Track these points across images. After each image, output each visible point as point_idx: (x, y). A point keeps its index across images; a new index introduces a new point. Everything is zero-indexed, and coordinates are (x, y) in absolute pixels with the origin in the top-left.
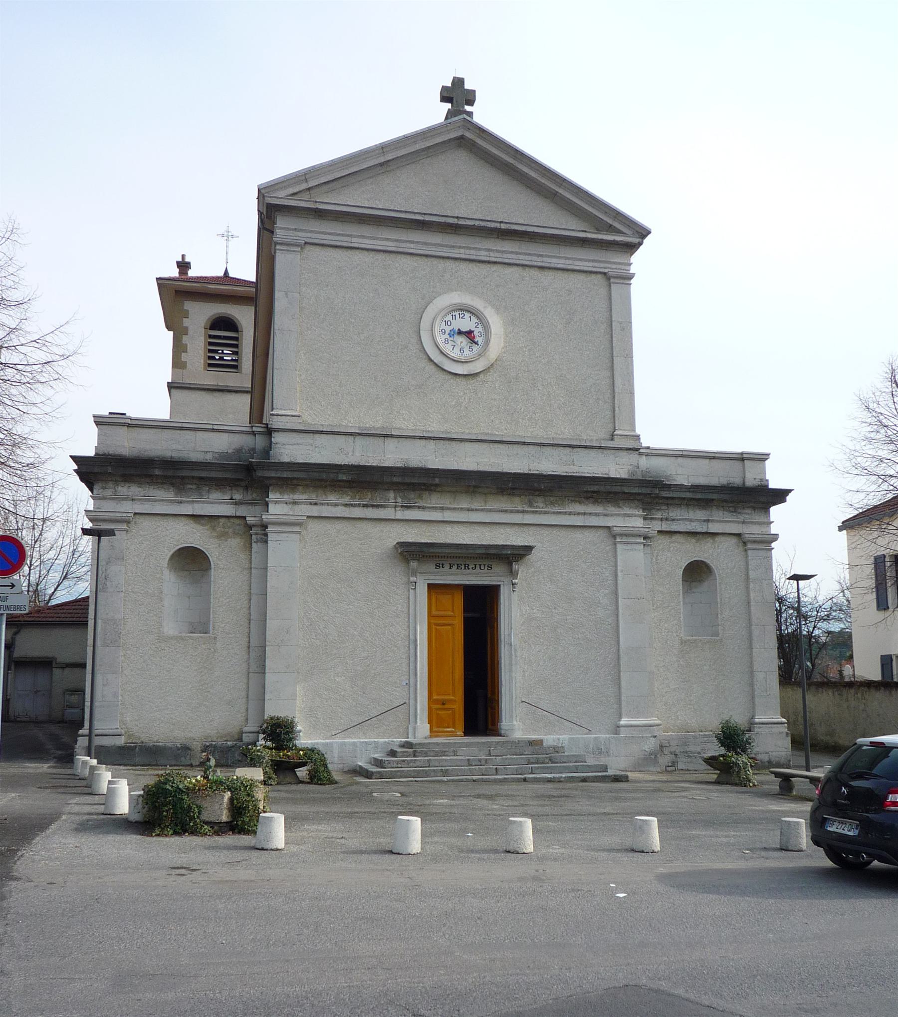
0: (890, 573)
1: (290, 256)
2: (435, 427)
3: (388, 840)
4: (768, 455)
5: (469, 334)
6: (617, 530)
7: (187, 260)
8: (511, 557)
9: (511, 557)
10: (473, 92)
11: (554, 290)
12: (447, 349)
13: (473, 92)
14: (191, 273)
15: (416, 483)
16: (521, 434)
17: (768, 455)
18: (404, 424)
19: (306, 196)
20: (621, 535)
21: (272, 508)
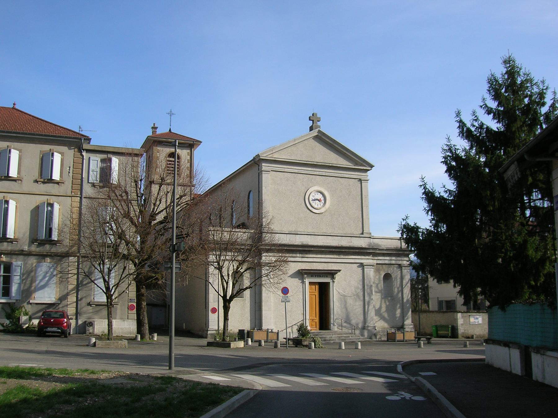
0: (482, 363)
1: (267, 175)
2: (310, 231)
3: (446, 332)
4: (372, 166)
5: (319, 200)
6: (365, 264)
7: (156, 126)
8: (332, 274)
9: (332, 274)
10: (320, 118)
11: (347, 183)
12: (313, 204)
13: (320, 118)
14: (159, 132)
15: (305, 250)
16: (336, 232)
17: (372, 166)
18: (301, 230)
19: (271, 155)
20: (366, 266)
21: (263, 258)
